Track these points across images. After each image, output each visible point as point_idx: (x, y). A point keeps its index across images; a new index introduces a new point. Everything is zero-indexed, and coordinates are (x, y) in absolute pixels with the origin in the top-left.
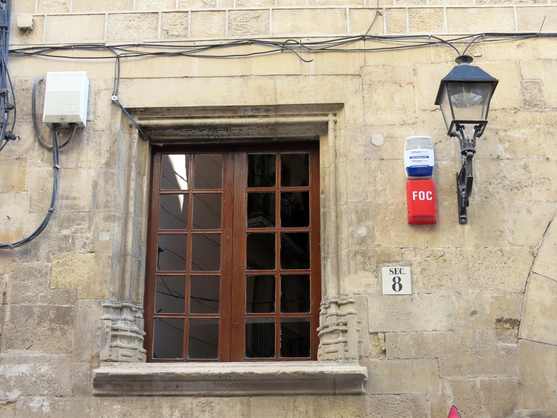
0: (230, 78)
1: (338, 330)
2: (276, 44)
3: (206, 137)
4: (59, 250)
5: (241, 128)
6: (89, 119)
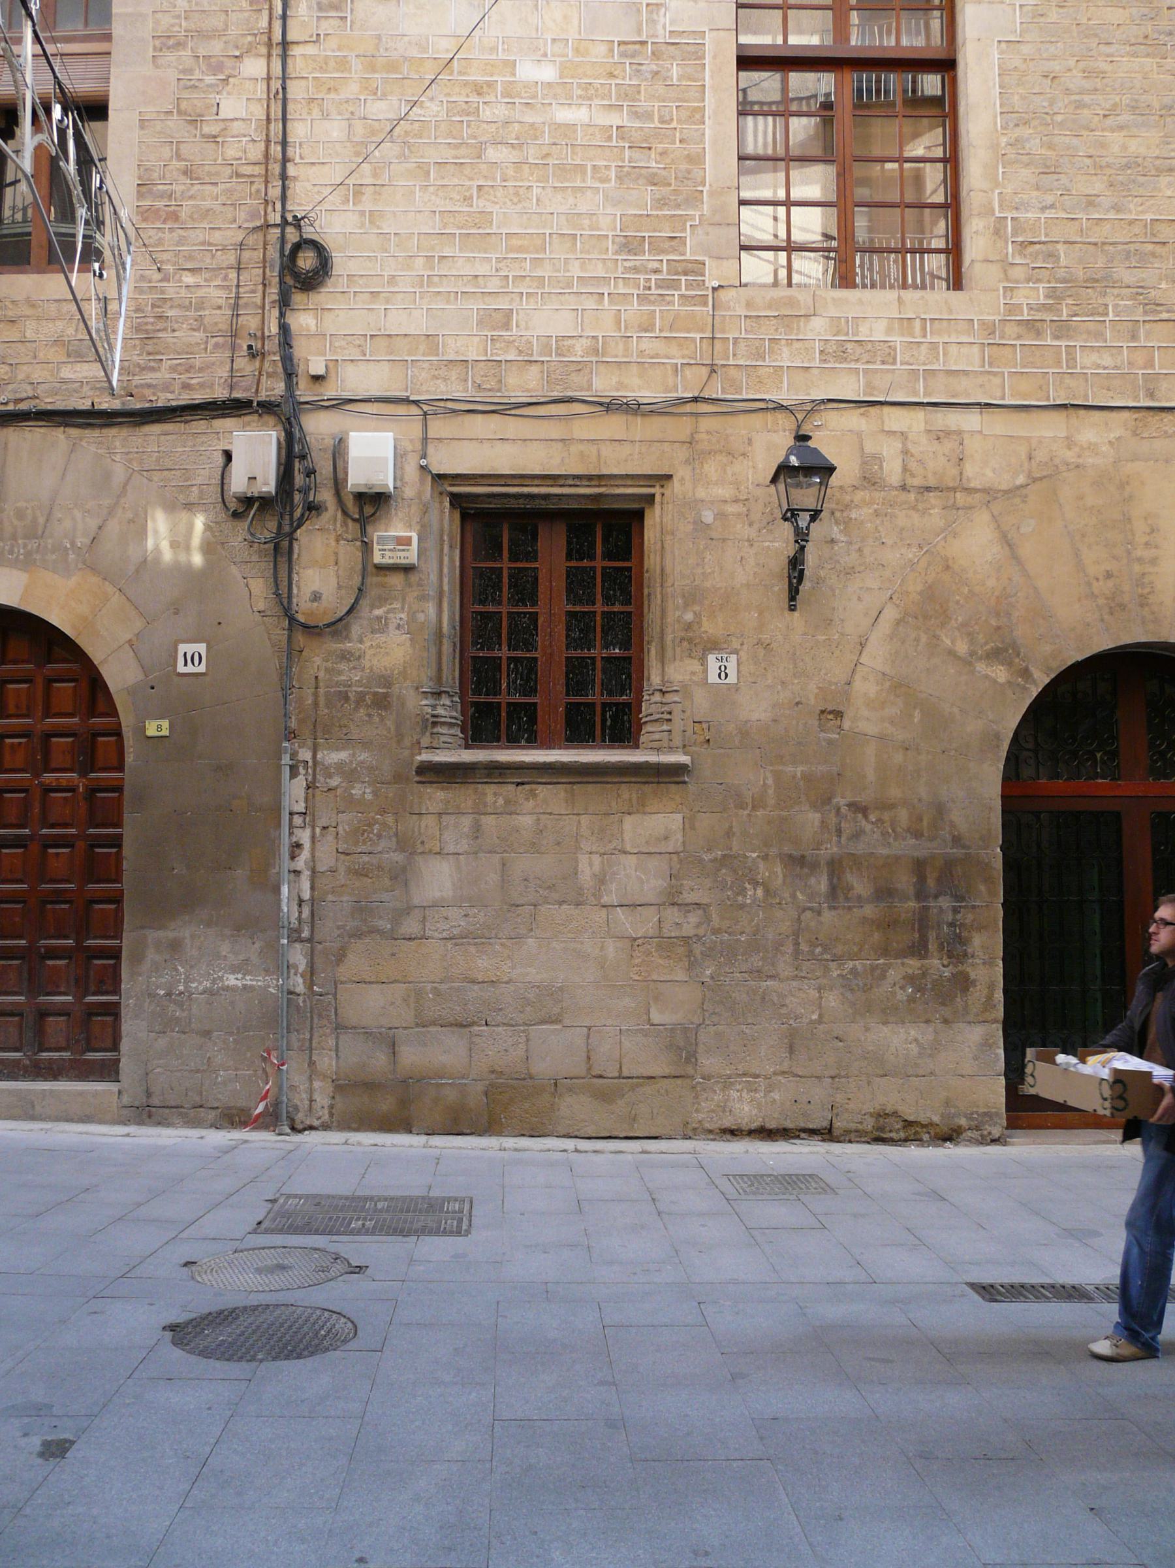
2: (601, 404)
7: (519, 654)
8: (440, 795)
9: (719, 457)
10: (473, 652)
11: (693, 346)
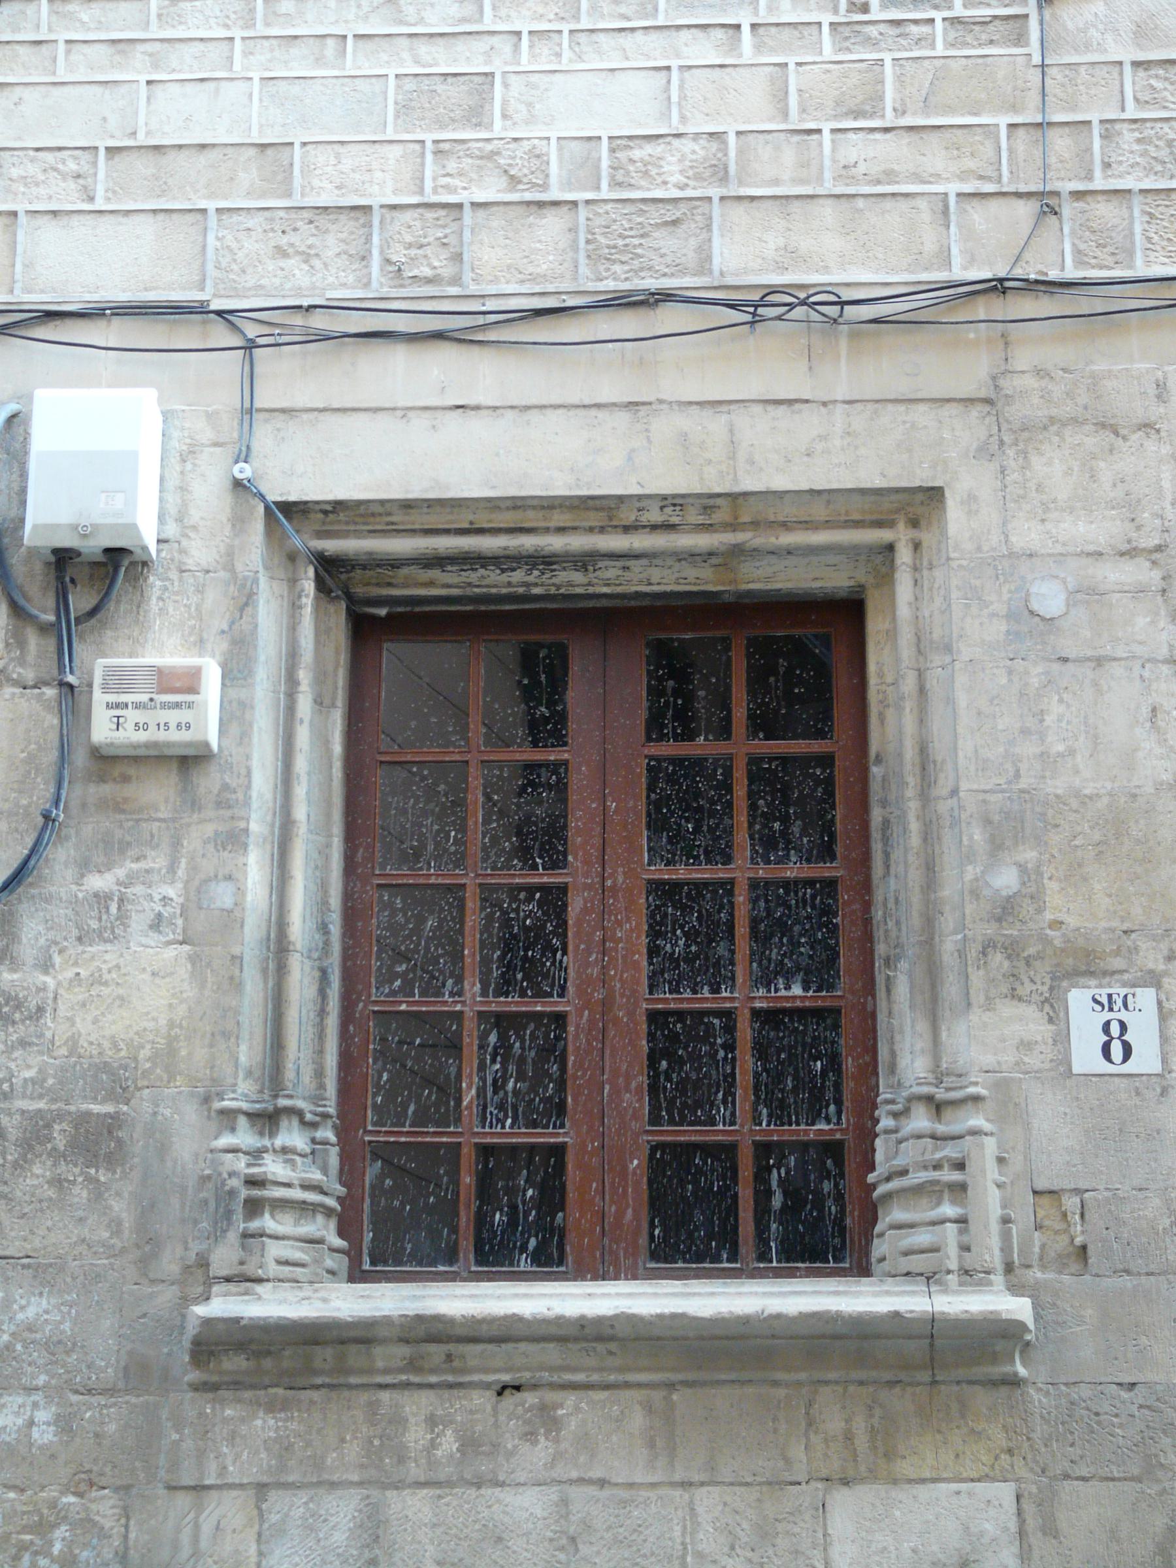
0: (593, 412)
1: (938, 1182)
3: (521, 590)
4: (79, 939)
5: (628, 563)
6: (163, 536)
7: (512, 1004)
8: (264, 1425)
9: (1072, 436)
10: (377, 997)
11: (988, 150)
